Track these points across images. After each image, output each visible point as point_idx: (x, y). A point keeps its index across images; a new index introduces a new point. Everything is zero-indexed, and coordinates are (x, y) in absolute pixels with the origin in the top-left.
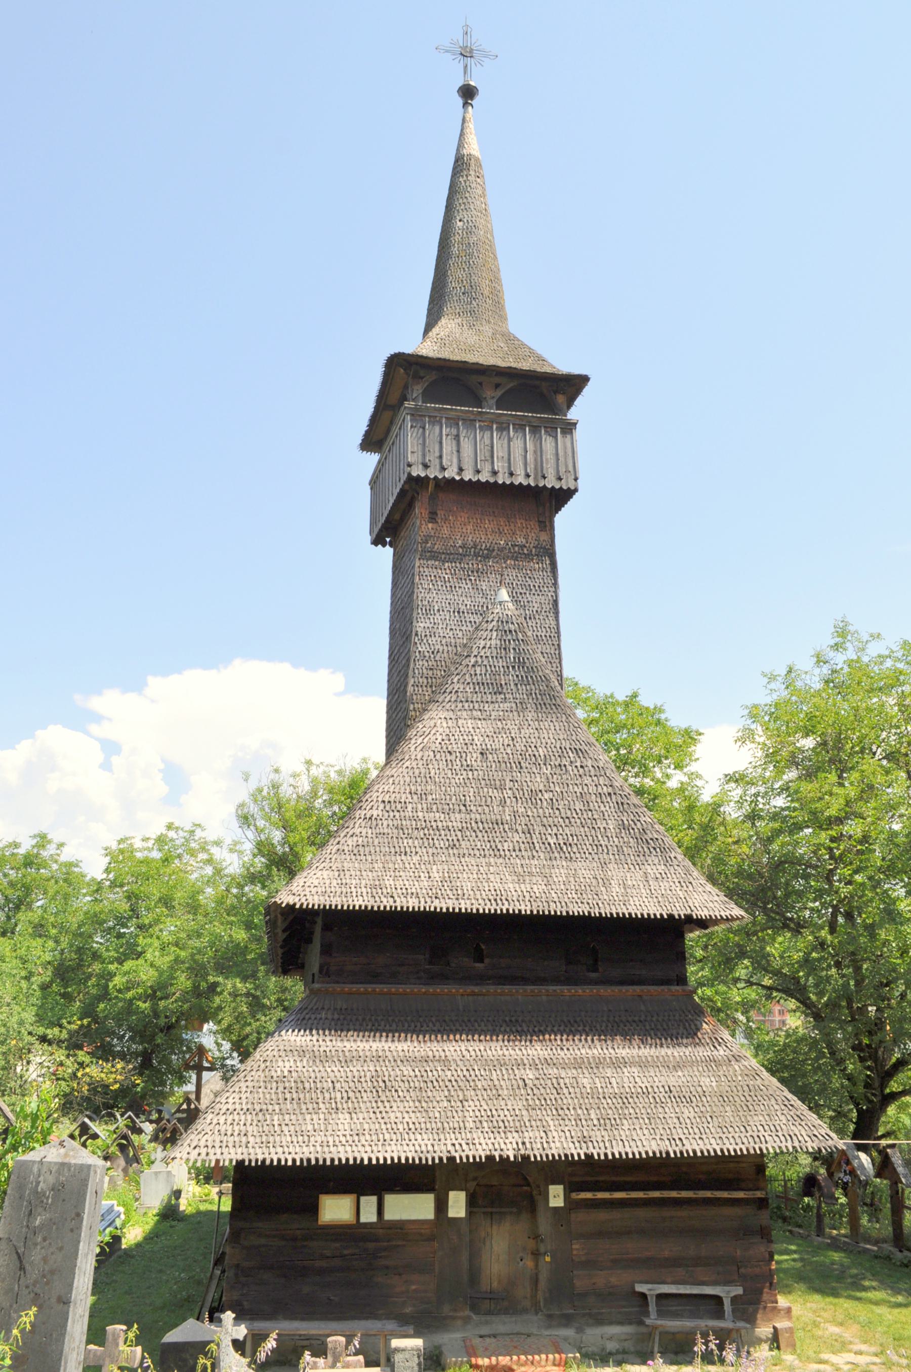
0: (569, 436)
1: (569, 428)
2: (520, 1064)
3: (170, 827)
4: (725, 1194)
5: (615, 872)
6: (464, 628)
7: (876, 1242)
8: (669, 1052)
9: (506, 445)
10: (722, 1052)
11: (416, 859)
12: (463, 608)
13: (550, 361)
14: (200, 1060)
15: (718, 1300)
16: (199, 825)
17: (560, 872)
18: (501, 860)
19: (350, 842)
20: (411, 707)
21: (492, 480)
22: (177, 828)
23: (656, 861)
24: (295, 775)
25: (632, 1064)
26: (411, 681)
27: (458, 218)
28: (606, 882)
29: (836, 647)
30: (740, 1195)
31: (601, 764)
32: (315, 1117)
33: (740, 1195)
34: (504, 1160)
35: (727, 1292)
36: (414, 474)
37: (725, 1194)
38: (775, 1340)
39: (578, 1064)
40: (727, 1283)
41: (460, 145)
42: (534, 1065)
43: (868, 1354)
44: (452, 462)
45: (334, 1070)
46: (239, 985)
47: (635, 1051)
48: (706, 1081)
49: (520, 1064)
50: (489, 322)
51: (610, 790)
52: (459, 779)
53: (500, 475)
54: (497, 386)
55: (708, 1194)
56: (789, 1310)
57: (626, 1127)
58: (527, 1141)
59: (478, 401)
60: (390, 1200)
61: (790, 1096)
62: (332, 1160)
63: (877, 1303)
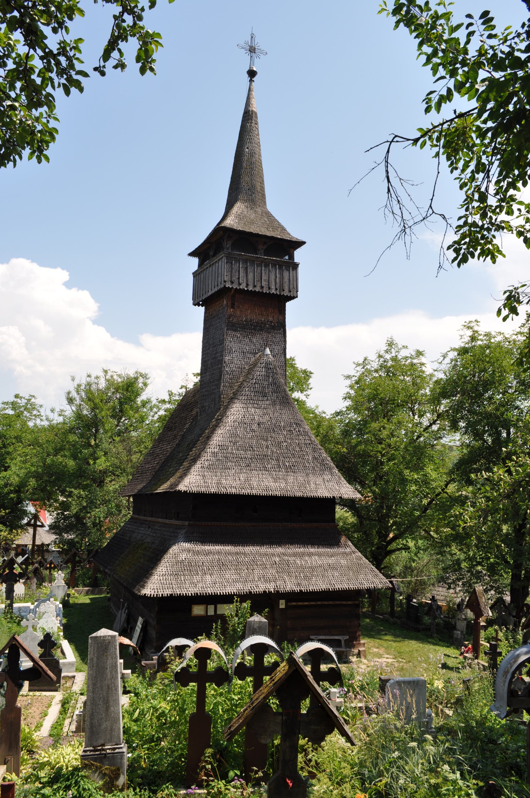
1: (295, 266)
2: (273, 555)
3: (17, 396)
5: (312, 478)
6: (245, 360)
7: (382, 614)
8: (329, 550)
9: (267, 274)
10: (348, 550)
11: (234, 471)
13: (287, 230)
14: (35, 522)
15: (339, 641)
16: (34, 396)
17: (291, 479)
18: (267, 472)
19: (206, 463)
20: (222, 396)
21: (261, 291)
22: (21, 397)
23: (328, 474)
24: (97, 377)
25: (316, 555)
26: (223, 384)
27: (246, 147)
29: (386, 351)
30: (350, 603)
31: (306, 430)
32: (197, 576)
33: (350, 603)
34: (270, 592)
35: (343, 638)
36: (227, 286)
37: (345, 603)
38: (359, 655)
39: (295, 555)
42: (279, 556)
43: (391, 658)
44: (243, 281)
45: (202, 558)
46: (82, 493)
47: (316, 550)
48: (342, 561)
49: (273, 555)
50: (260, 206)
51: (310, 442)
52: (249, 435)
53: (265, 288)
54: (265, 243)
55: (338, 603)
56: (364, 644)
57: (314, 580)
58: (278, 585)
60: (219, 606)
61: (373, 567)
62: (206, 593)
63: (390, 641)
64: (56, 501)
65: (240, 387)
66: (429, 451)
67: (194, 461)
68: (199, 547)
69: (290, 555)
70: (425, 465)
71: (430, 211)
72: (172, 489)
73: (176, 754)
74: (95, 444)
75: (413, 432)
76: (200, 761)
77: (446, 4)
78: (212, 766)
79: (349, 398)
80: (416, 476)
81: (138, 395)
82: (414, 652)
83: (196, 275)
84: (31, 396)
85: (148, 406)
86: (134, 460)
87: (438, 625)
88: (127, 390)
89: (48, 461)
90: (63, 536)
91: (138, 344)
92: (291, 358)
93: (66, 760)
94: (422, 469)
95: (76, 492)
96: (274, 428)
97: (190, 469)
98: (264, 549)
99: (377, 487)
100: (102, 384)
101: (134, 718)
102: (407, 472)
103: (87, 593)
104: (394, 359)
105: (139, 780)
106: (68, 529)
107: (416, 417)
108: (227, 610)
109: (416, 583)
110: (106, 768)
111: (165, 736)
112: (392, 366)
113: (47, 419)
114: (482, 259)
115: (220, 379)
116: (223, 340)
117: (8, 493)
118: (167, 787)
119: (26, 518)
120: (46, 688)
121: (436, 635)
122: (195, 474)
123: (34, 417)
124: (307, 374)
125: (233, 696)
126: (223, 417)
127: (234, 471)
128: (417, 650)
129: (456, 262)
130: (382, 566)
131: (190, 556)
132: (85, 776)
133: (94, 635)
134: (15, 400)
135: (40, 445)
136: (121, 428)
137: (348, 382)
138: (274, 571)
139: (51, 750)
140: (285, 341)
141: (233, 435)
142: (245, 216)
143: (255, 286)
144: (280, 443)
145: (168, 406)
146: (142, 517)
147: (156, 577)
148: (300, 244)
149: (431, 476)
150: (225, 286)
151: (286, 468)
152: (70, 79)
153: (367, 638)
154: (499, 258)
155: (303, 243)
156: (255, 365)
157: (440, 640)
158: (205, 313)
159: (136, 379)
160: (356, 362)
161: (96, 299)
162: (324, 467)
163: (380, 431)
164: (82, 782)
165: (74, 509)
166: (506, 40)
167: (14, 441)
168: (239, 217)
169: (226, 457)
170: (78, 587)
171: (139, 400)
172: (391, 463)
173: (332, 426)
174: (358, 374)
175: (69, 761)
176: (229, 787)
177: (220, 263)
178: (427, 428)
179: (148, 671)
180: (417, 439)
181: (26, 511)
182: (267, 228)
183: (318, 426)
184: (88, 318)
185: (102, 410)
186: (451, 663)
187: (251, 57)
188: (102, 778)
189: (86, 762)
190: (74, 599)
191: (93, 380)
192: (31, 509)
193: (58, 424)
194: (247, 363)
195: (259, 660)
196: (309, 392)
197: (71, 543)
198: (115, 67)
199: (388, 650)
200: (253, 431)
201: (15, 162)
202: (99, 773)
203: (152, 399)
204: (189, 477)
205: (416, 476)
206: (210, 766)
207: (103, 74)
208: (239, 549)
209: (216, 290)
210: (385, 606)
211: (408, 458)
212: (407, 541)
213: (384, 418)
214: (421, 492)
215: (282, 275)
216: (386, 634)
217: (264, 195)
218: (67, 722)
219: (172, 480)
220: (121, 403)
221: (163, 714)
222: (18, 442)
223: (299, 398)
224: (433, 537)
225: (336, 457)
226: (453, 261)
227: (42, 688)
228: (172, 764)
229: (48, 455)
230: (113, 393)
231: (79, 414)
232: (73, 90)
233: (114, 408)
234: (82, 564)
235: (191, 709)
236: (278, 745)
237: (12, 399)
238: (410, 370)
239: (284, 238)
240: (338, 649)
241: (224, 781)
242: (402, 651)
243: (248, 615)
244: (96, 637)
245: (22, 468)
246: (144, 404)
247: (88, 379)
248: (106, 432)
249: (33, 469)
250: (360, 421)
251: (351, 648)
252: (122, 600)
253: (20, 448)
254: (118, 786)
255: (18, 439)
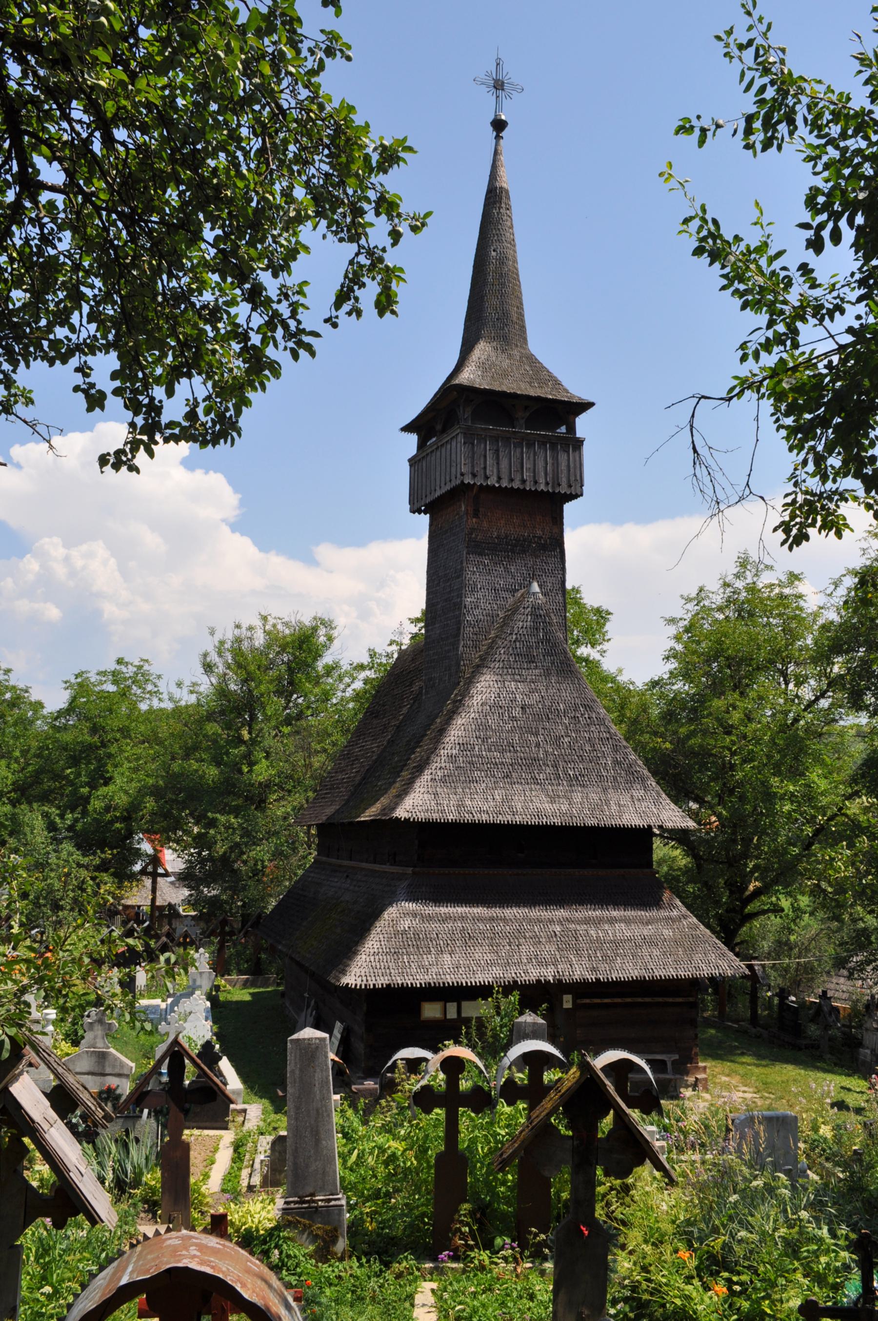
0: (577, 453)
2: (551, 921)
4: (671, 1000)
5: (612, 795)
7: (736, 1021)
11: (484, 785)
12: (498, 586)
14: (155, 869)
15: (663, 1062)
16: (147, 661)
21: (522, 487)
24: (250, 628)
25: (621, 921)
28: (608, 804)
29: (737, 576)
30: (680, 1000)
33: (680, 1000)
35: (669, 1058)
36: (466, 482)
37: (671, 1000)
38: (695, 1086)
39: (587, 921)
40: (669, 1052)
41: (494, 175)
42: (560, 922)
47: (622, 913)
48: (666, 932)
49: (551, 921)
52: (508, 727)
53: (528, 483)
54: (526, 408)
55: (660, 1000)
56: (705, 1068)
59: (512, 423)
60: (465, 1004)
61: (717, 941)
63: (749, 1065)
64: (188, 832)
65: (490, 647)
66: (814, 745)
67: (420, 769)
68: (431, 909)
69: (579, 922)
70: (807, 769)
71: (747, 492)
72: (385, 815)
73: (416, 1213)
74: (250, 739)
75: (786, 713)
76: (452, 1221)
77: (764, 224)
78: (471, 1229)
79: (675, 657)
80: (791, 788)
81: (318, 656)
82: (791, 1083)
83: (413, 462)
84: (142, 660)
85: (335, 674)
86: (317, 765)
87: (831, 1039)
88: (300, 648)
89: (176, 767)
90: (202, 892)
91: (311, 561)
92: (573, 589)
93: (256, 1220)
94: (802, 774)
95: (222, 819)
96: (548, 714)
97: (414, 782)
98: (536, 913)
99: (724, 808)
100: (260, 639)
101: (349, 1164)
102: (775, 781)
103: (245, 985)
104: (752, 589)
105: (365, 1247)
106: (209, 879)
107: (791, 686)
108: (481, 1009)
109: (797, 970)
110: (318, 1227)
111: (397, 1190)
112: (748, 601)
113: (171, 699)
114: (824, 533)
115: (458, 635)
116: (462, 569)
117: (112, 822)
118: (406, 1258)
119: (140, 863)
120: (208, 1124)
121: (829, 1056)
122: (422, 790)
123: (148, 696)
124: (602, 616)
125: (498, 1130)
126: (464, 697)
127: (484, 785)
128: (795, 1080)
129: (787, 545)
130: (738, 940)
131: (416, 922)
132: (289, 1238)
133: (295, 1036)
134: (118, 667)
135: (160, 743)
136: (292, 711)
137: (672, 630)
138: (553, 948)
139: (232, 1205)
140: (563, 569)
141: (482, 727)
142: (494, 364)
143: (512, 480)
144: (558, 738)
145: (370, 674)
146: (333, 861)
147: (364, 957)
148: (585, 406)
149: (818, 787)
150: (462, 482)
151: (570, 779)
152: (300, 343)
153: (710, 1060)
154: (846, 533)
155: (590, 405)
156: (514, 610)
157: (836, 1065)
158: (431, 525)
159: (315, 629)
160: (685, 596)
161: (236, 489)
162: (632, 778)
163: (728, 712)
164: (285, 1246)
165: (221, 849)
166: (833, 290)
167: (118, 735)
168: (484, 367)
169: (471, 763)
170: (229, 975)
171: (320, 665)
172: (748, 767)
173: (645, 704)
174: (690, 615)
175: (259, 1222)
176: (496, 1260)
177: (454, 443)
178: (811, 704)
179: (362, 1100)
180: (792, 724)
181: (140, 849)
182: (530, 383)
183: (622, 707)
184: (223, 520)
185: (261, 682)
186: (851, 1100)
187: (497, 97)
188: (313, 1242)
189: (290, 1218)
190: (225, 994)
191: (244, 633)
192: (146, 847)
193: (187, 707)
194: (501, 607)
195: (535, 1076)
196: (606, 646)
197: (214, 902)
198: (349, 314)
199: (745, 1079)
200: (514, 719)
201: (233, 440)
202: (309, 1234)
203: (342, 663)
204: (412, 796)
205: (791, 788)
206: (467, 1229)
207: (335, 325)
208: (496, 912)
209: (448, 487)
210: (742, 1007)
211: (778, 757)
212: (778, 899)
213: (734, 691)
214: (801, 815)
215: (555, 459)
216: (743, 1054)
217: (523, 328)
218: (245, 1173)
219: (384, 801)
220: (291, 671)
221: (393, 1158)
222: (125, 737)
223: (589, 655)
224: (824, 891)
225: (653, 758)
226: (783, 544)
227: (202, 1125)
228: (411, 1225)
229: (173, 758)
230: (278, 653)
231: (224, 691)
232: (302, 352)
233: (280, 679)
234: (234, 938)
235: (436, 1147)
236: (567, 1200)
237: (112, 666)
238: (778, 606)
239: (559, 398)
240: (662, 1076)
241: (488, 1252)
242: (769, 1080)
243: (516, 1013)
244: (298, 1040)
245: (132, 780)
246: (329, 670)
247: (237, 632)
248: (267, 719)
249: (151, 781)
250: (694, 695)
251: (682, 1074)
252: (306, 995)
253: (129, 748)
254: (336, 1254)
255: (125, 732)
